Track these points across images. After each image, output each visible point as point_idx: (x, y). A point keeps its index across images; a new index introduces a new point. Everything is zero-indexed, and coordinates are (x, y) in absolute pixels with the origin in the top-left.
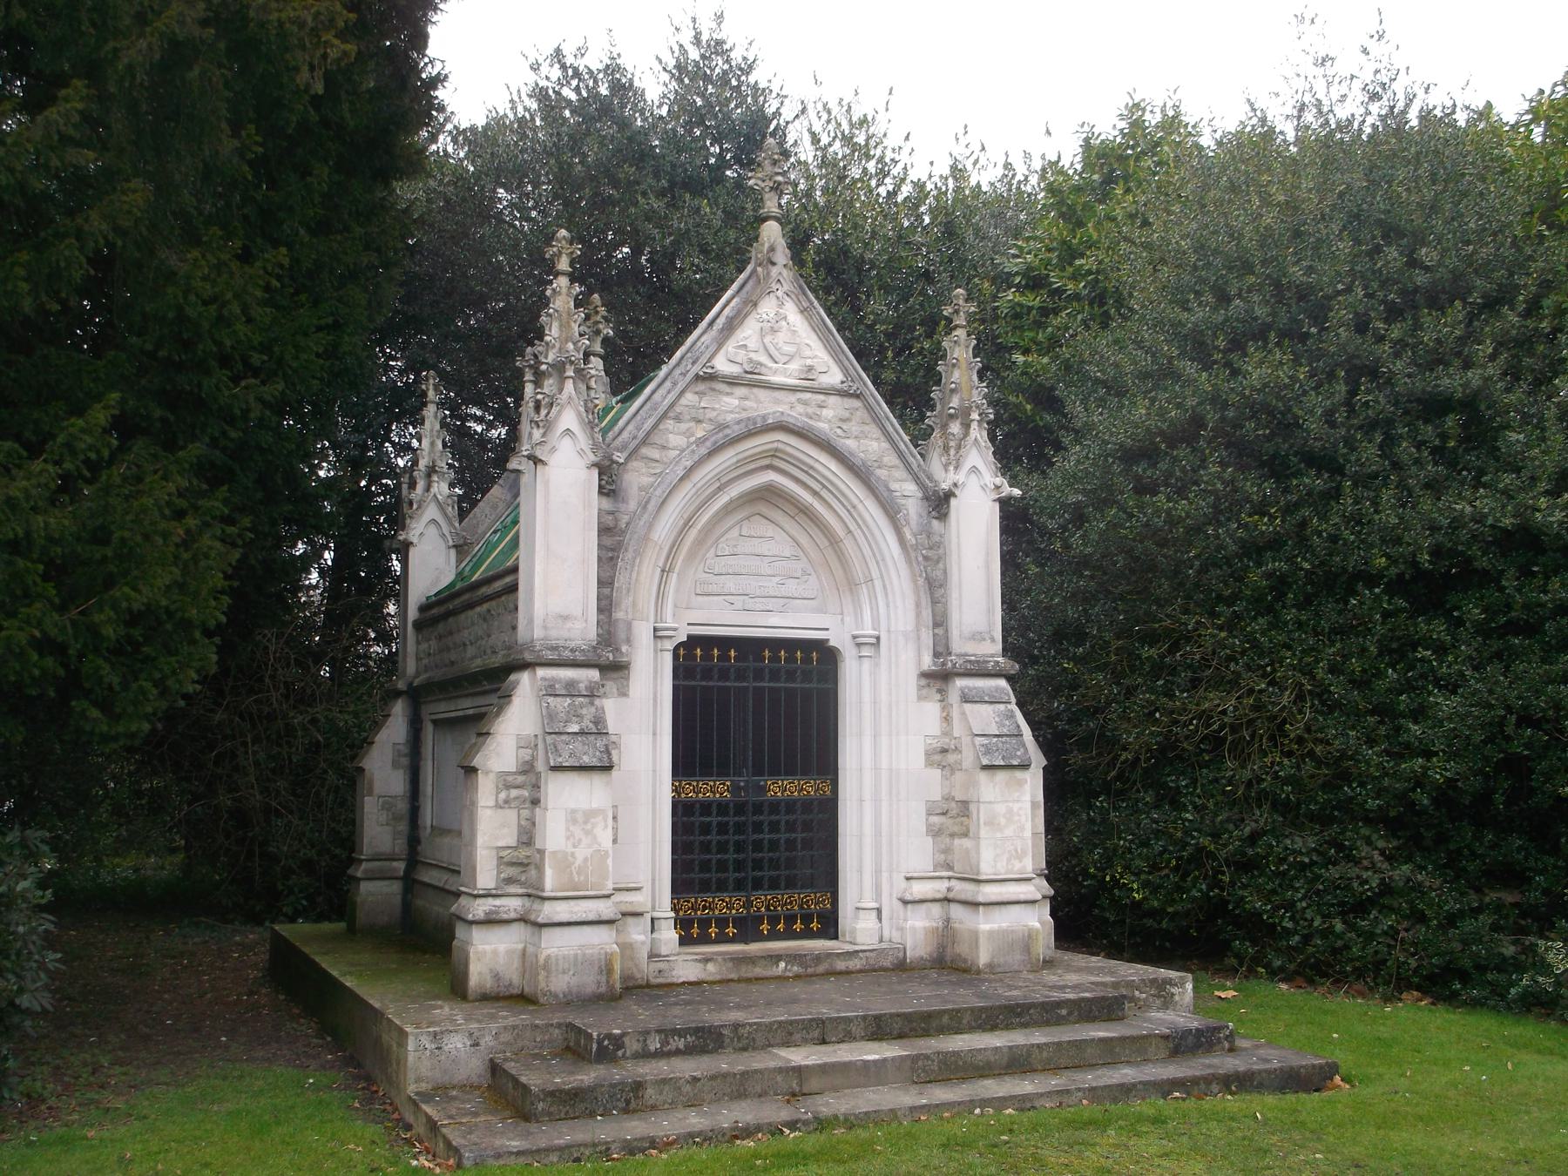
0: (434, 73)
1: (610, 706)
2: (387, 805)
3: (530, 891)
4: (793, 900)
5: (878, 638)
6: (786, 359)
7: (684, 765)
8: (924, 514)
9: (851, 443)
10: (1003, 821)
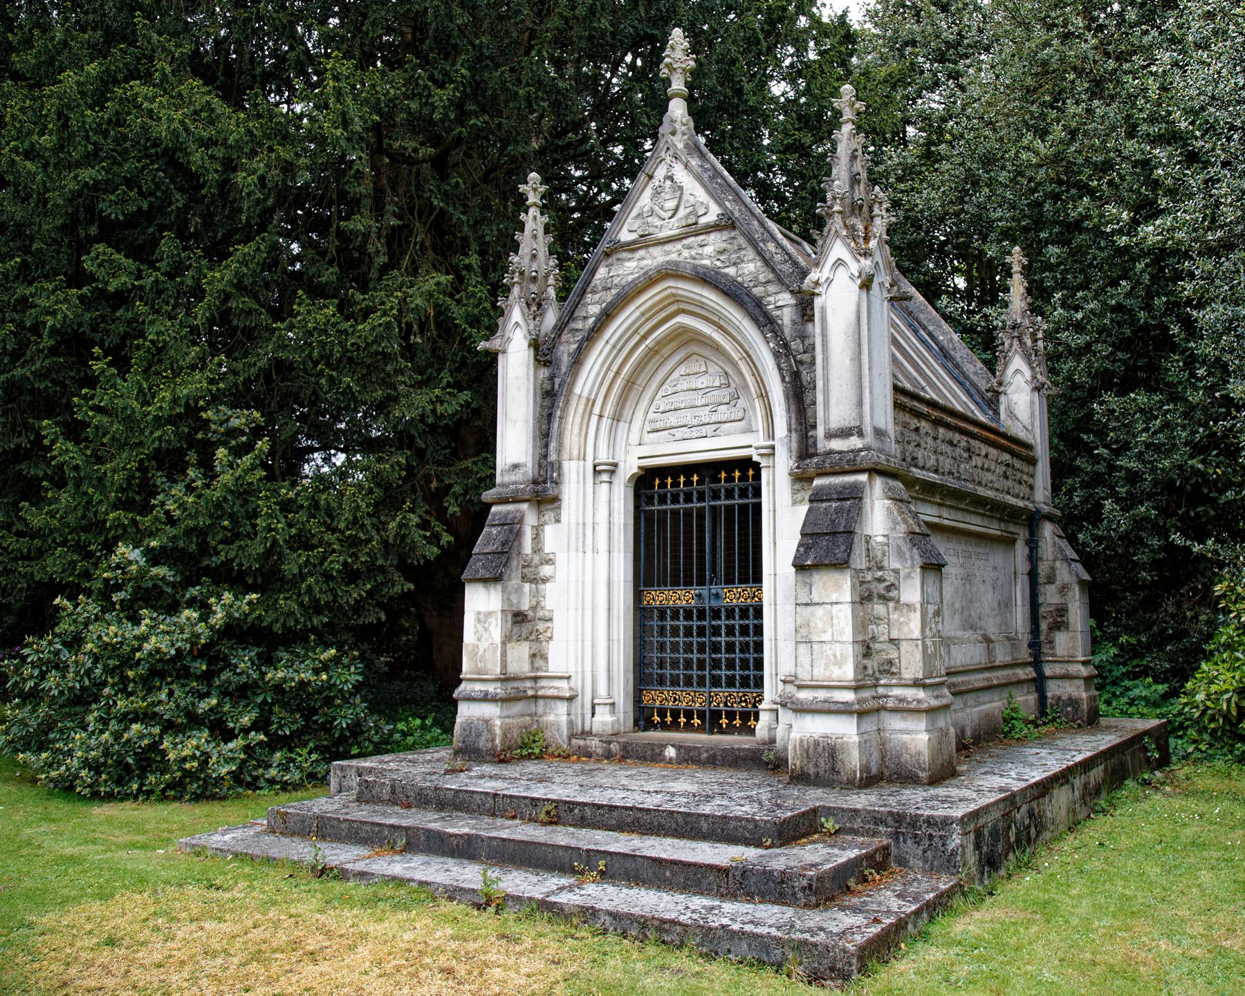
4: (721, 697)
6: (670, 213)
9: (731, 271)
10: (820, 625)
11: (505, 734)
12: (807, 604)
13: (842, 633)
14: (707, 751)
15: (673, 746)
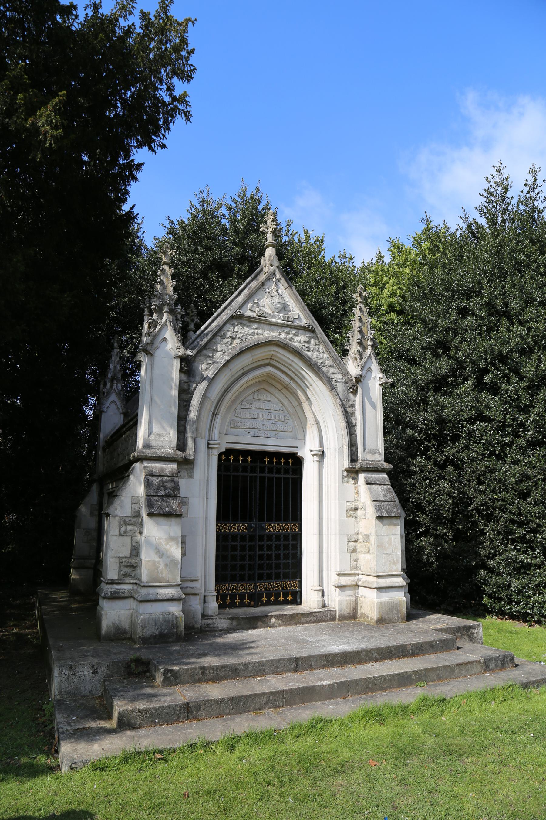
1: (183, 483)
3: (136, 581)
7: (224, 514)
9: (309, 354)
10: (387, 545)
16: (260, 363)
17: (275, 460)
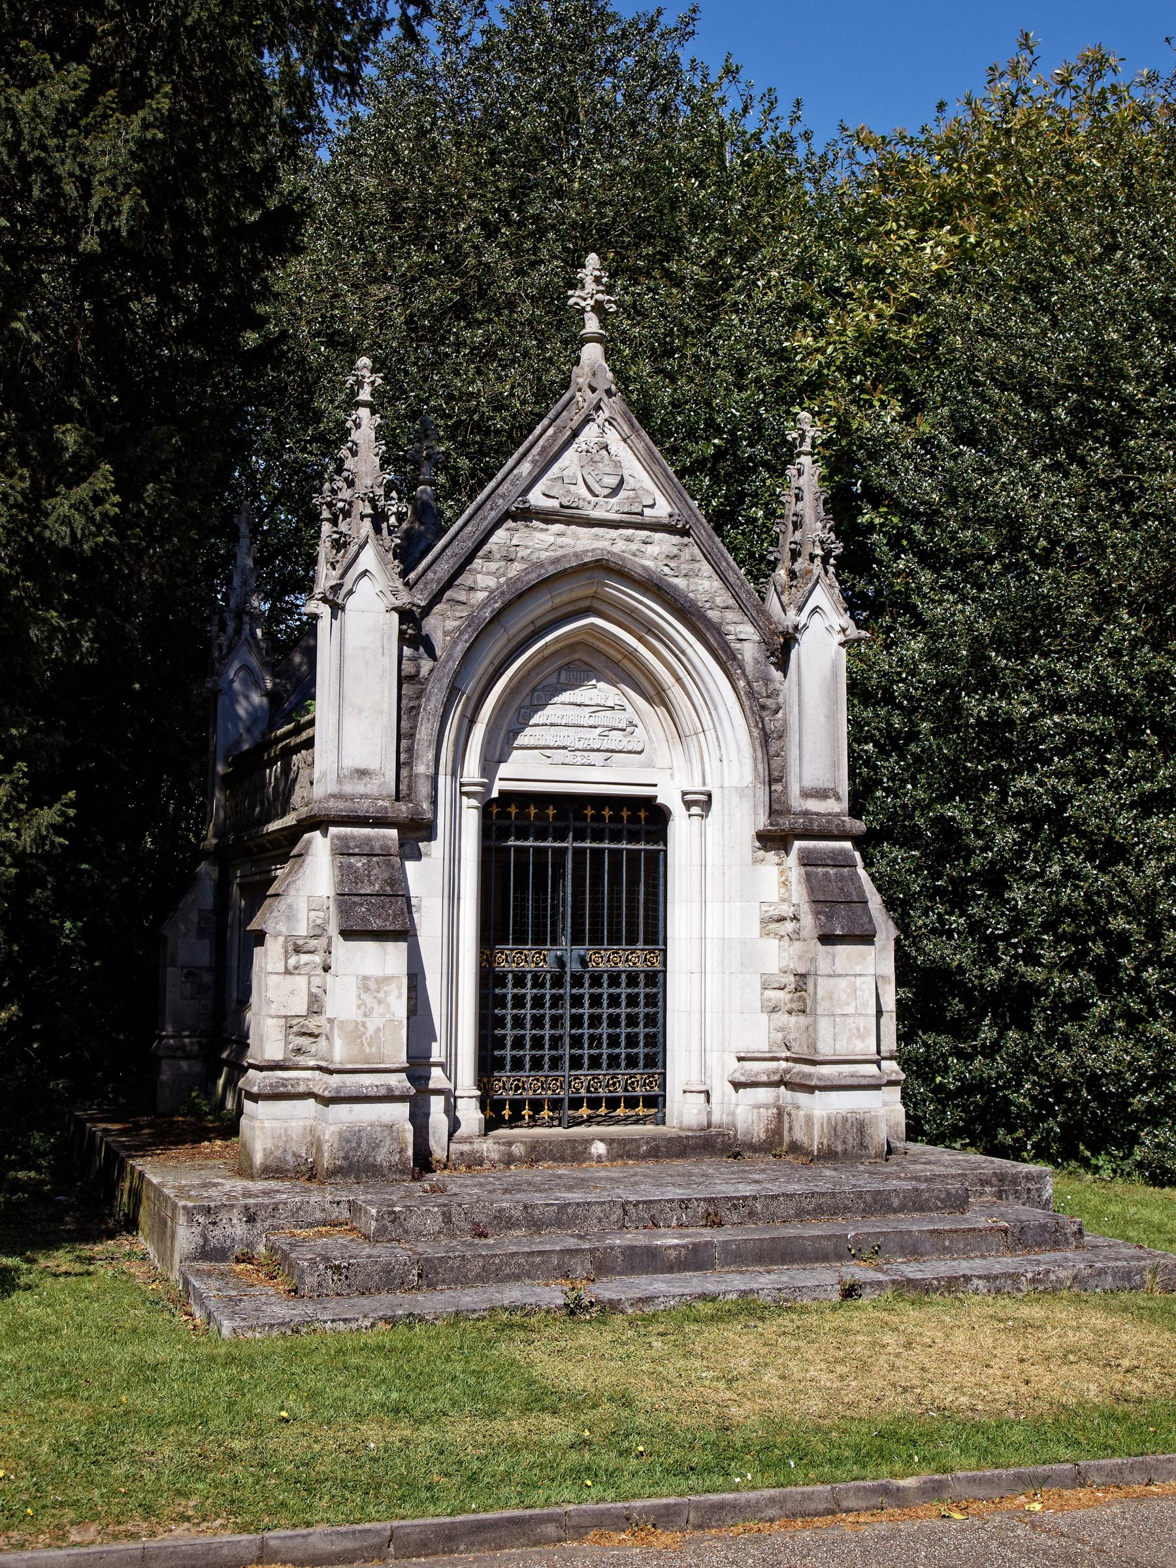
0: (28, 91)
2: (191, 974)
5: (710, 796)
6: (609, 491)
8: (762, 659)
9: (680, 582)
10: (844, 997)
11: (266, 1156)
12: (829, 976)
13: (866, 1005)
14: (647, 1143)
15: (602, 1140)
16: (571, 608)
17: (607, 813)
